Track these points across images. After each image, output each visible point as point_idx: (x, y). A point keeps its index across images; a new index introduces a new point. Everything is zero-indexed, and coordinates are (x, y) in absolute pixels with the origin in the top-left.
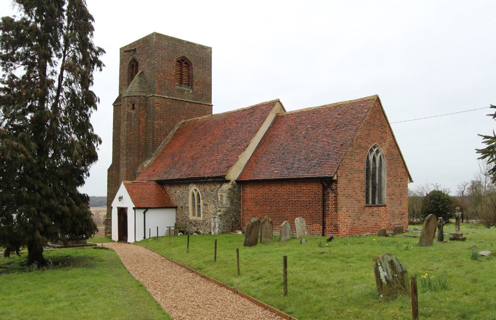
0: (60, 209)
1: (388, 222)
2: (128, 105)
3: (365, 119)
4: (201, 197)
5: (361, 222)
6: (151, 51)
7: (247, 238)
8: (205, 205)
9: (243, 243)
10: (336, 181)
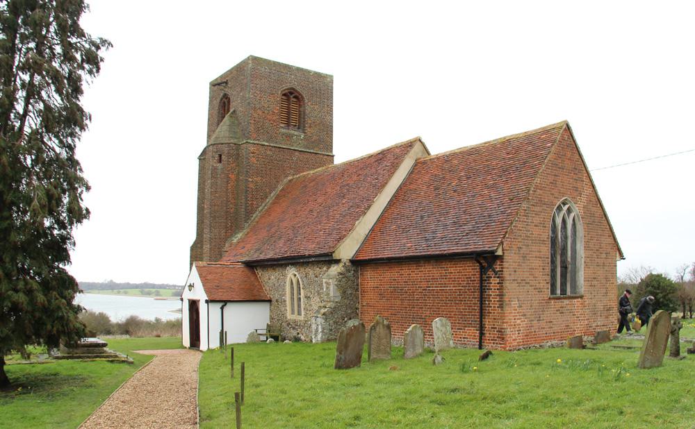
0: (9, 297)
1: (586, 322)
2: (213, 157)
3: (548, 158)
4: (301, 286)
5: (543, 324)
6: (245, 81)
7: (340, 353)
8: (307, 297)
9: (334, 362)
10: (501, 258)
